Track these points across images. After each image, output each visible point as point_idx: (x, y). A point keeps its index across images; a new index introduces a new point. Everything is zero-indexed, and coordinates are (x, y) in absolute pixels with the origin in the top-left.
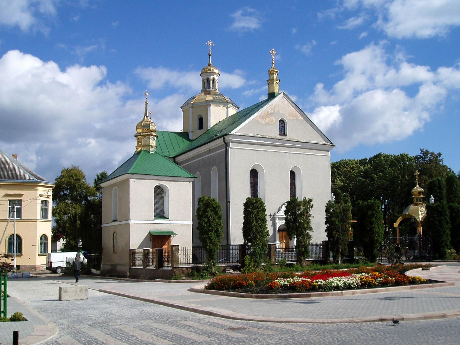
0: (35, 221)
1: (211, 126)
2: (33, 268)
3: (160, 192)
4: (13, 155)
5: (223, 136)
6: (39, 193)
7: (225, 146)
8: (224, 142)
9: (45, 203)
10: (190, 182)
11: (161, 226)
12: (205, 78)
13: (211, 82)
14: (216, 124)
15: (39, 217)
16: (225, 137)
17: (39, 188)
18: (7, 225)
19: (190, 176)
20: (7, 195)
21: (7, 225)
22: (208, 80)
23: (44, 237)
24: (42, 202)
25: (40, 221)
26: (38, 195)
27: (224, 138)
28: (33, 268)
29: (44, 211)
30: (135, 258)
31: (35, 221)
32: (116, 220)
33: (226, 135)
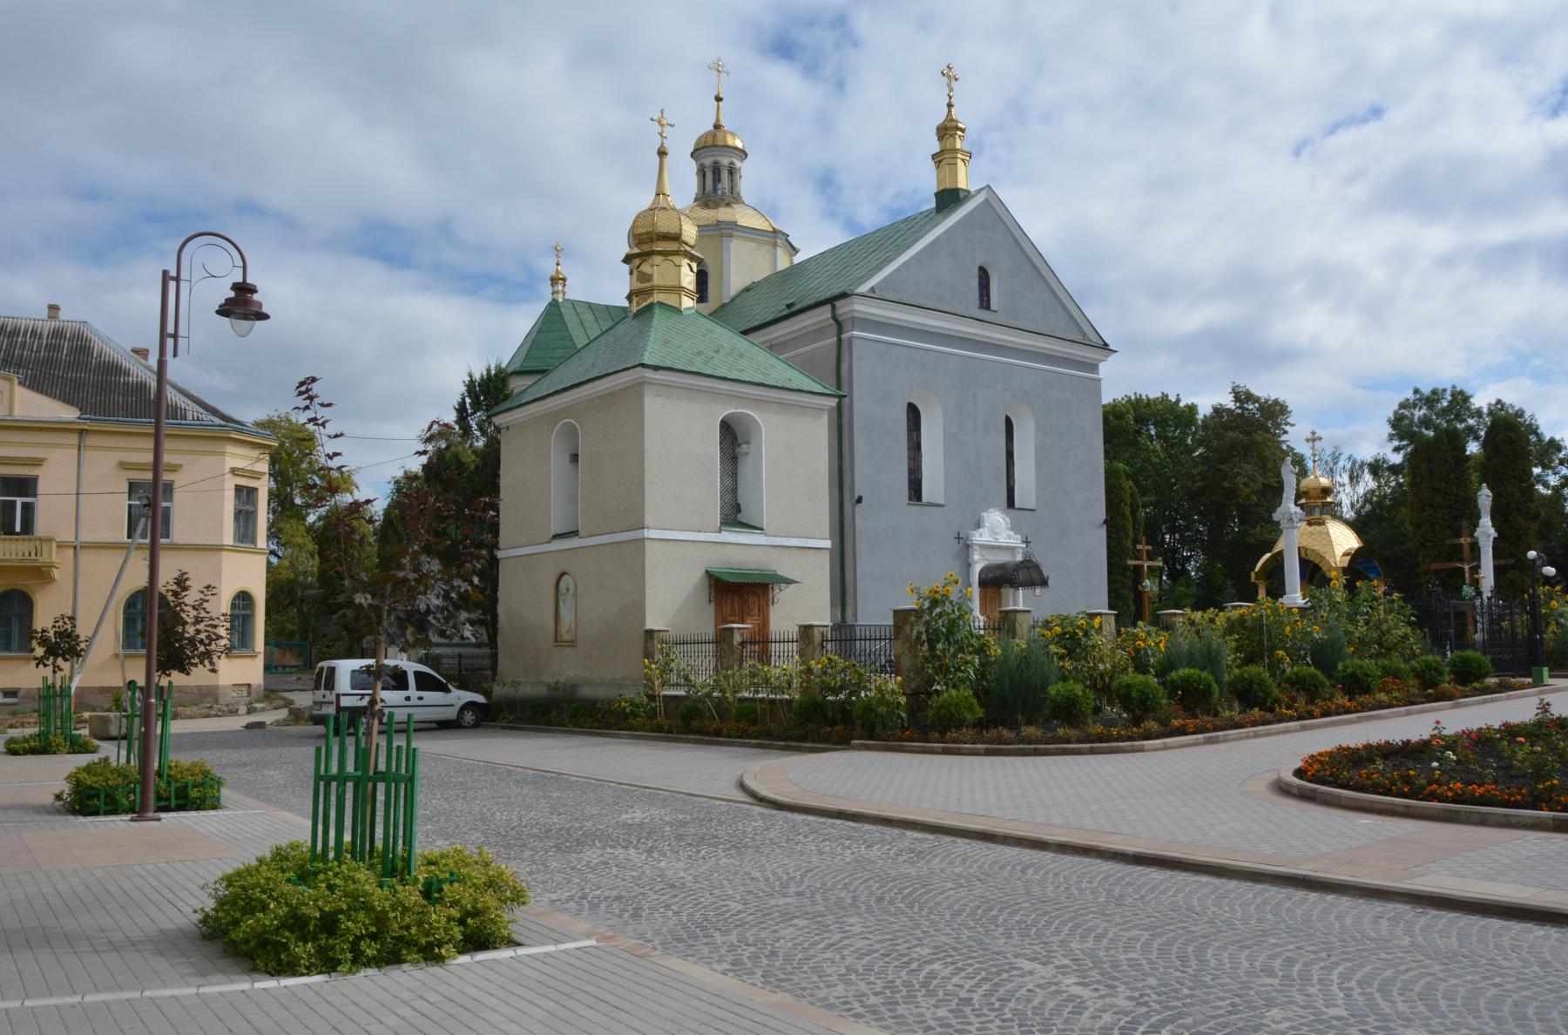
0: (219, 548)
1: (733, 293)
2: (206, 695)
3: (732, 437)
4: (136, 351)
5: (831, 301)
6: (231, 462)
7: (835, 327)
8: (834, 317)
9: (245, 495)
10: (820, 409)
11: (741, 551)
12: (708, 161)
13: (725, 175)
14: (747, 289)
15: (228, 538)
16: (838, 304)
17: (230, 448)
18: (125, 561)
19: (819, 389)
20: (124, 466)
21: (125, 561)
22: (716, 169)
23: (243, 599)
24: (239, 489)
25: (231, 549)
26: (227, 470)
27: (834, 308)
28: (206, 695)
29: (245, 518)
30: (801, 653)
31: (219, 548)
32: (574, 533)
33: (844, 295)
